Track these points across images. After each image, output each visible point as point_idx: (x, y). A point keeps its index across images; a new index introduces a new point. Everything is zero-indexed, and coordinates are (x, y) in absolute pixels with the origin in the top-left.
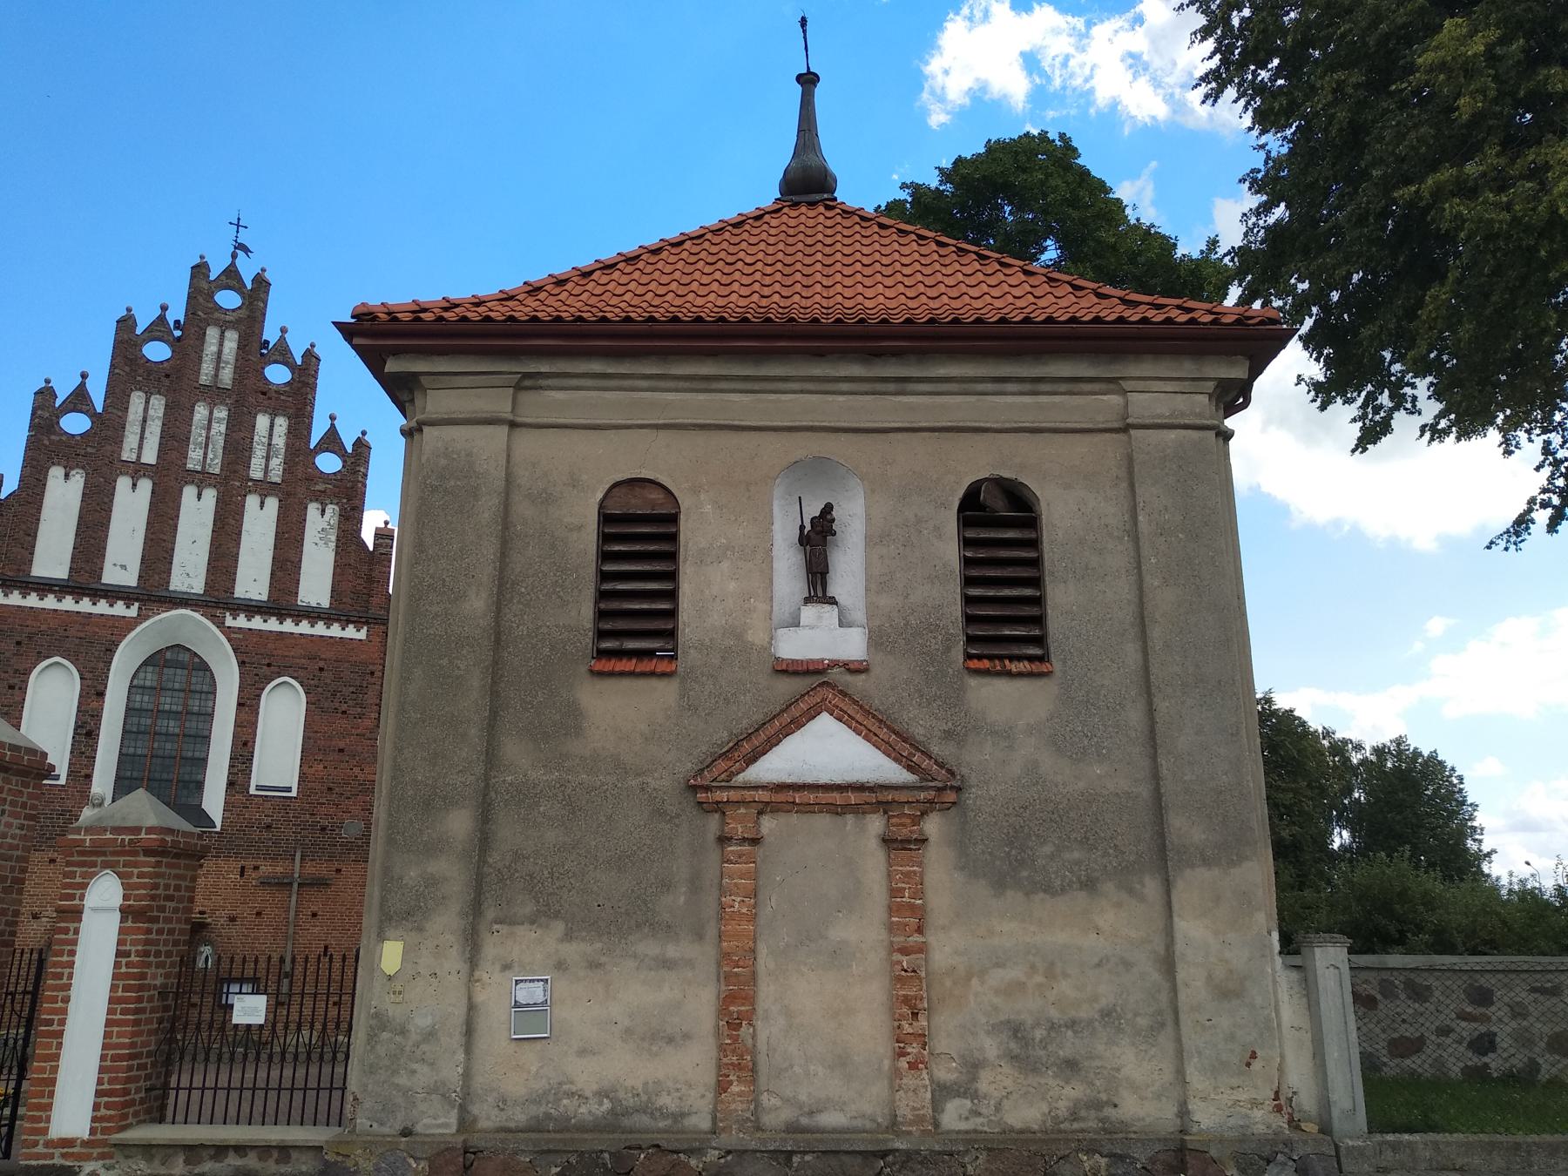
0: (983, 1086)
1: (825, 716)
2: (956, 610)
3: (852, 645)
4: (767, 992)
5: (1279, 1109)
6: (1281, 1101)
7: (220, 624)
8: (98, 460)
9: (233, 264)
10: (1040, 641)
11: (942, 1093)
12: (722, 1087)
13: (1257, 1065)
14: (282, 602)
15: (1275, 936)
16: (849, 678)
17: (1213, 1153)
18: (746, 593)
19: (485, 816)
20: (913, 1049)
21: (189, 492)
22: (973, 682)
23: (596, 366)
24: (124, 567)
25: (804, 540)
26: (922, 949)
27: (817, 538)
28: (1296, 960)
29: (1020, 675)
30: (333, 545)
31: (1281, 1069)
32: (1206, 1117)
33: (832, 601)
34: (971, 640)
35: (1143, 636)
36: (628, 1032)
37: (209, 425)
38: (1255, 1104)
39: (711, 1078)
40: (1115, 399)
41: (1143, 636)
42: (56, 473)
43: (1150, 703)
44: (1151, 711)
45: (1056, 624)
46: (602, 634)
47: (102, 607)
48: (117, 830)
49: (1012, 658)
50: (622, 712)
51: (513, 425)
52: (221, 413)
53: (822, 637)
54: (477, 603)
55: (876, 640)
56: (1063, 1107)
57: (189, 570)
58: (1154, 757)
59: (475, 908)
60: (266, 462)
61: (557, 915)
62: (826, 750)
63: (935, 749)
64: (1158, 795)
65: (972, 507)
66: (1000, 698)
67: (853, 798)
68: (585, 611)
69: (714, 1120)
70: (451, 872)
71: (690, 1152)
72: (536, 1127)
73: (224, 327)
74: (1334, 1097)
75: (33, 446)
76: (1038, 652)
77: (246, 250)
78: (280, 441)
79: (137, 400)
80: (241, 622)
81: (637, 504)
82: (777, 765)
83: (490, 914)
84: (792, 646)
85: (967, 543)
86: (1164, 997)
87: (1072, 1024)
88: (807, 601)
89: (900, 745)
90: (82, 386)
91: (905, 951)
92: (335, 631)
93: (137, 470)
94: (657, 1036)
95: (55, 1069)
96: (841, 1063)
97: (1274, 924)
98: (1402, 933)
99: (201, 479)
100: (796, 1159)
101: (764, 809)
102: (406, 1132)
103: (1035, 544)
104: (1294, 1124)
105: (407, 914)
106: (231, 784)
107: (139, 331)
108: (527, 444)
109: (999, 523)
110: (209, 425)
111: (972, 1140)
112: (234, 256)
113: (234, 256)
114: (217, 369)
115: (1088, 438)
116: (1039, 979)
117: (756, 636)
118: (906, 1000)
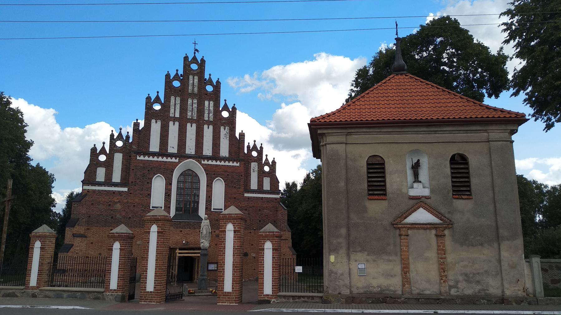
0: (459, 286)
1: (421, 210)
2: (450, 184)
3: (426, 192)
4: (412, 267)
5: (524, 291)
6: (525, 290)
7: (200, 163)
8: (164, 117)
9: (195, 56)
10: (469, 191)
11: (451, 287)
12: (403, 285)
13: (519, 282)
14: (216, 156)
15: (523, 255)
16: (426, 200)
17: (510, 300)
18: (397, 178)
19: (348, 230)
20: (444, 278)
21: (189, 125)
22: (454, 200)
23: (364, 130)
24: (173, 148)
25: (413, 167)
26: (445, 258)
27: (416, 167)
28: (528, 260)
29: (465, 199)
30: (228, 138)
31: (525, 283)
32: (508, 293)
33: (420, 182)
34: (453, 191)
35: (493, 190)
36: (383, 274)
37: (192, 104)
38: (519, 290)
39: (401, 283)
40: (486, 134)
41: (493, 190)
42: (153, 121)
43: (495, 205)
44: (495, 207)
45: (473, 187)
46: (369, 190)
47: (169, 160)
48: (269, 232)
49: (463, 195)
50: (375, 207)
51: (346, 144)
52: (195, 101)
53: (418, 190)
54: (342, 184)
55: (432, 191)
56: (477, 290)
57: (190, 148)
58: (496, 217)
59: (348, 249)
60: (208, 116)
61: (365, 251)
62: (422, 216)
63: (446, 216)
64: (497, 225)
65: (453, 160)
66: (460, 204)
67: (429, 226)
68: (365, 185)
69: (402, 292)
70: (343, 241)
71: (398, 298)
72: (365, 293)
73: (194, 75)
74: (536, 289)
75: (147, 114)
76: (469, 193)
77: (198, 51)
78: (212, 108)
79: (173, 98)
80: (206, 162)
81: (374, 161)
82: (411, 219)
83: (351, 250)
84: (413, 193)
85: (452, 168)
86: (498, 268)
87: (478, 274)
88: (414, 182)
89: (439, 215)
90: (158, 96)
91: (441, 258)
92: (231, 164)
93: (174, 119)
94: (388, 275)
95: (263, 281)
96: (428, 281)
97: (523, 252)
98: (559, 251)
99: (192, 121)
100: (420, 300)
101: (409, 228)
102: (339, 294)
103: (468, 168)
104: (528, 295)
105: (334, 250)
106: (206, 208)
107: (171, 78)
108: (350, 148)
109: (459, 163)
110: (192, 104)
111: (457, 296)
112: (195, 53)
113: (195, 53)
114: (193, 88)
115: (480, 143)
116: (471, 264)
117: (404, 190)
118: (442, 268)
